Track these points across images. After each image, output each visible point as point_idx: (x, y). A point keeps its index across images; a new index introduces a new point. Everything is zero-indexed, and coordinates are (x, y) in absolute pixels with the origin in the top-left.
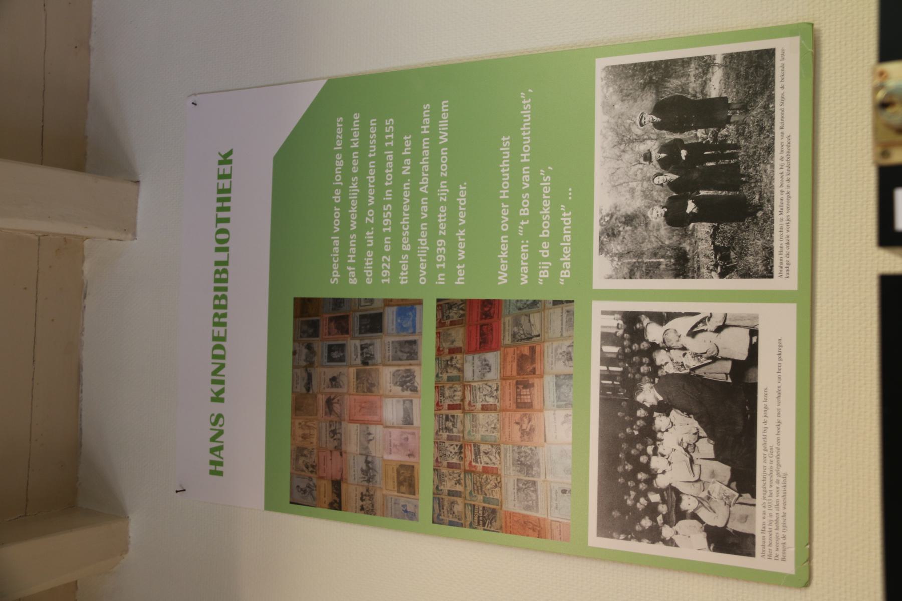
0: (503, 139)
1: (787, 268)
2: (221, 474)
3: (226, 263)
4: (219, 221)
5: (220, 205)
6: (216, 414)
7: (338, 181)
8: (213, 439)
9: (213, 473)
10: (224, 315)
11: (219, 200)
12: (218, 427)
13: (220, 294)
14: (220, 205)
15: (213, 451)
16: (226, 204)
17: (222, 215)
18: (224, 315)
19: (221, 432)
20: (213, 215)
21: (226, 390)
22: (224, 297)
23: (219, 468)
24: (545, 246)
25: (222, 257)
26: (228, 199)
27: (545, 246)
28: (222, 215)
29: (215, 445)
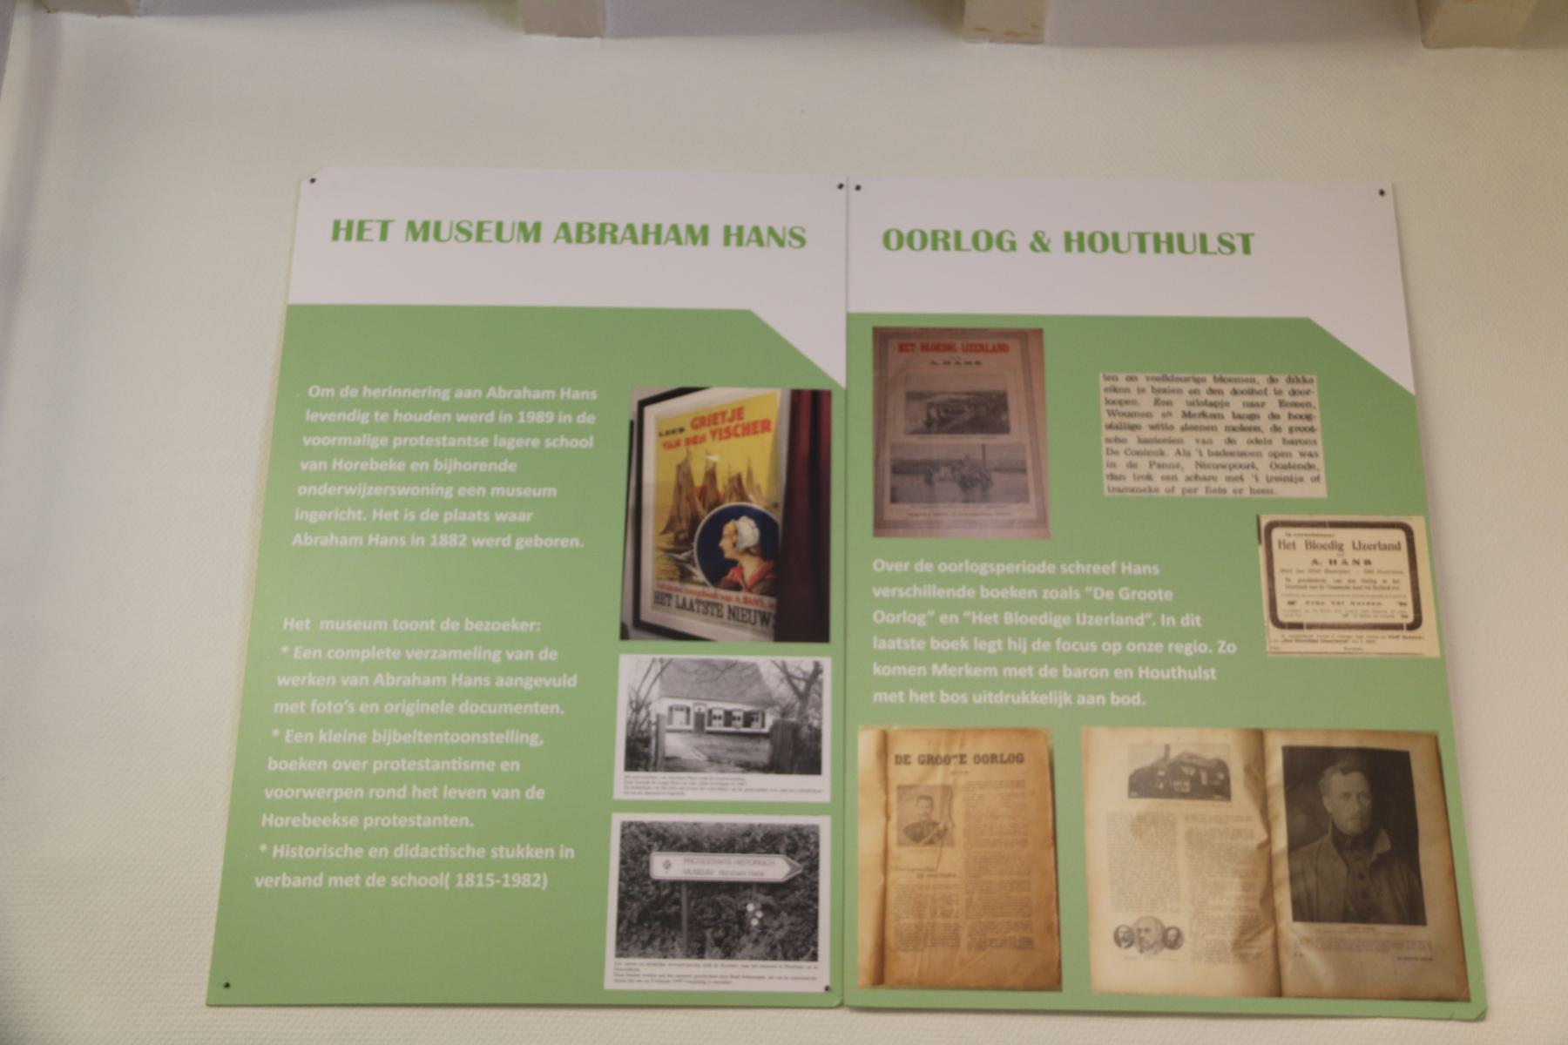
0: (1213, 671)
1: (1290, 479)
2: (336, 237)
3: (958, 247)
4: (1142, 237)
5: (1163, 238)
6: (804, 235)
7: (442, 880)
8: (771, 231)
9: (337, 224)
10: (947, 247)
11: (1169, 236)
12: (788, 238)
13: (596, 232)
14: (1163, 238)
15: (756, 230)
16: (1164, 247)
17: (1149, 241)
18: (947, 247)
19: (781, 243)
20: (1149, 227)
21: (569, 246)
22: (592, 240)
23: (734, 240)
24: (1053, 673)
25: (966, 242)
26: (1170, 250)
27: (1053, 673)
28: (1149, 241)
29: (764, 233)
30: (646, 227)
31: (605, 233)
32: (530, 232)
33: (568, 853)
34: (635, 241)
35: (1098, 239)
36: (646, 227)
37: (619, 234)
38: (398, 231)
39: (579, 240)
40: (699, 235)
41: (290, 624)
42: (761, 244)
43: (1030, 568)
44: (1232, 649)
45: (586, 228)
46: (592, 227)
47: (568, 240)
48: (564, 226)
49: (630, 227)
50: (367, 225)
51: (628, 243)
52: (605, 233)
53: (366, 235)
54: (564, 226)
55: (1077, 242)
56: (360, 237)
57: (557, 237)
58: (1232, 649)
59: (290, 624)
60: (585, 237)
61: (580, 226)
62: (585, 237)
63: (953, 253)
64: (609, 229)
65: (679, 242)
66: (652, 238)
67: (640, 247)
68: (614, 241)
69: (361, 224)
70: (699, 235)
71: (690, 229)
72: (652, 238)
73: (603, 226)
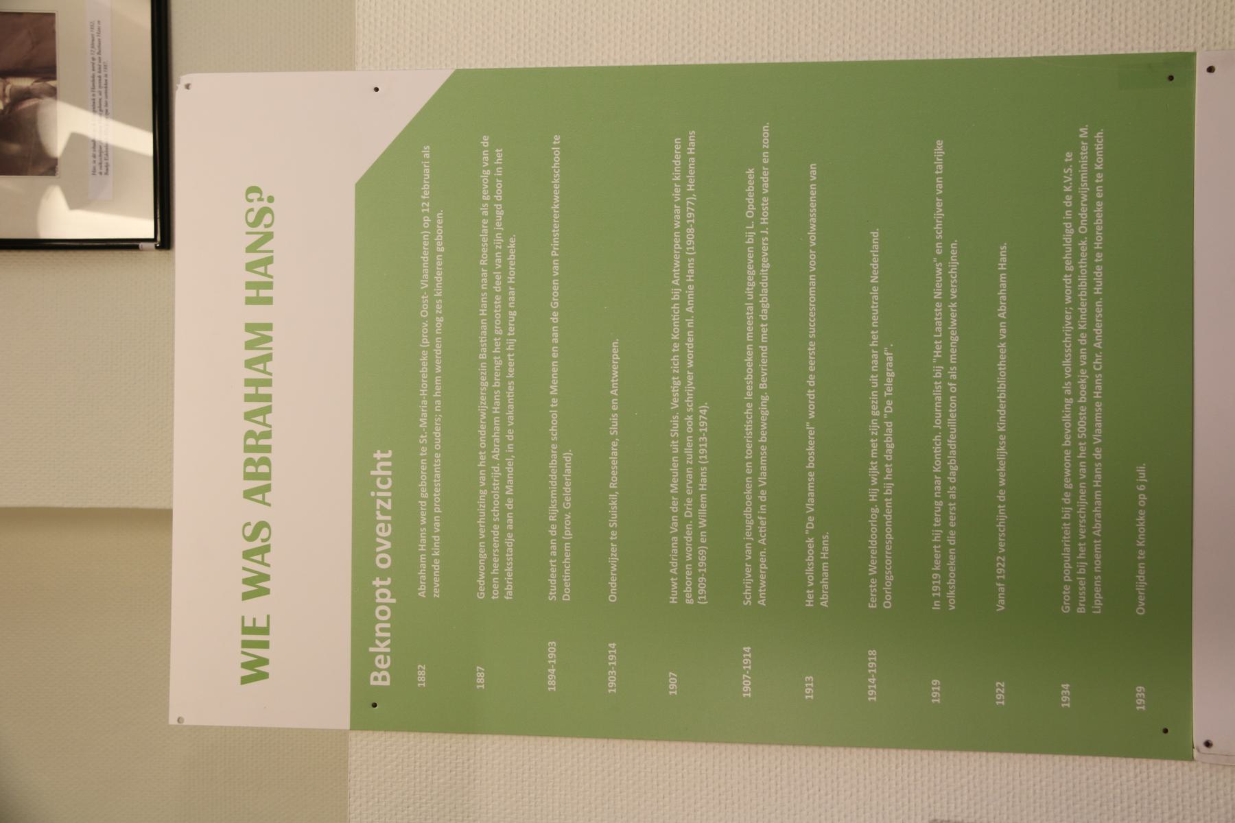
8: (251, 249)
12: (261, 228)
13: (256, 456)
19: (268, 236)
22: (266, 461)
30: (248, 398)
31: (258, 447)
32: (256, 586)
33: (485, 141)
34: (268, 410)
36: (248, 398)
37: (259, 429)
38: (256, 512)
39: (267, 476)
40: (259, 293)
41: (809, 603)
42: (269, 261)
43: (889, 570)
44: (486, 138)
45: (251, 469)
46: (249, 462)
47: (267, 488)
48: (248, 494)
49: (249, 416)
50: (249, 623)
51: (270, 418)
52: (258, 447)
53: (261, 623)
54: (248, 494)
56: (265, 631)
57: (263, 502)
58: (486, 138)
59: (809, 603)
60: (263, 469)
61: (248, 476)
62: (263, 469)
63: (273, 482)
64: (251, 442)
65: (269, 357)
66: (263, 390)
67: (274, 403)
68: (267, 435)
69: (245, 631)
70: (259, 293)
71: (249, 345)
72: (263, 390)
73: (248, 449)
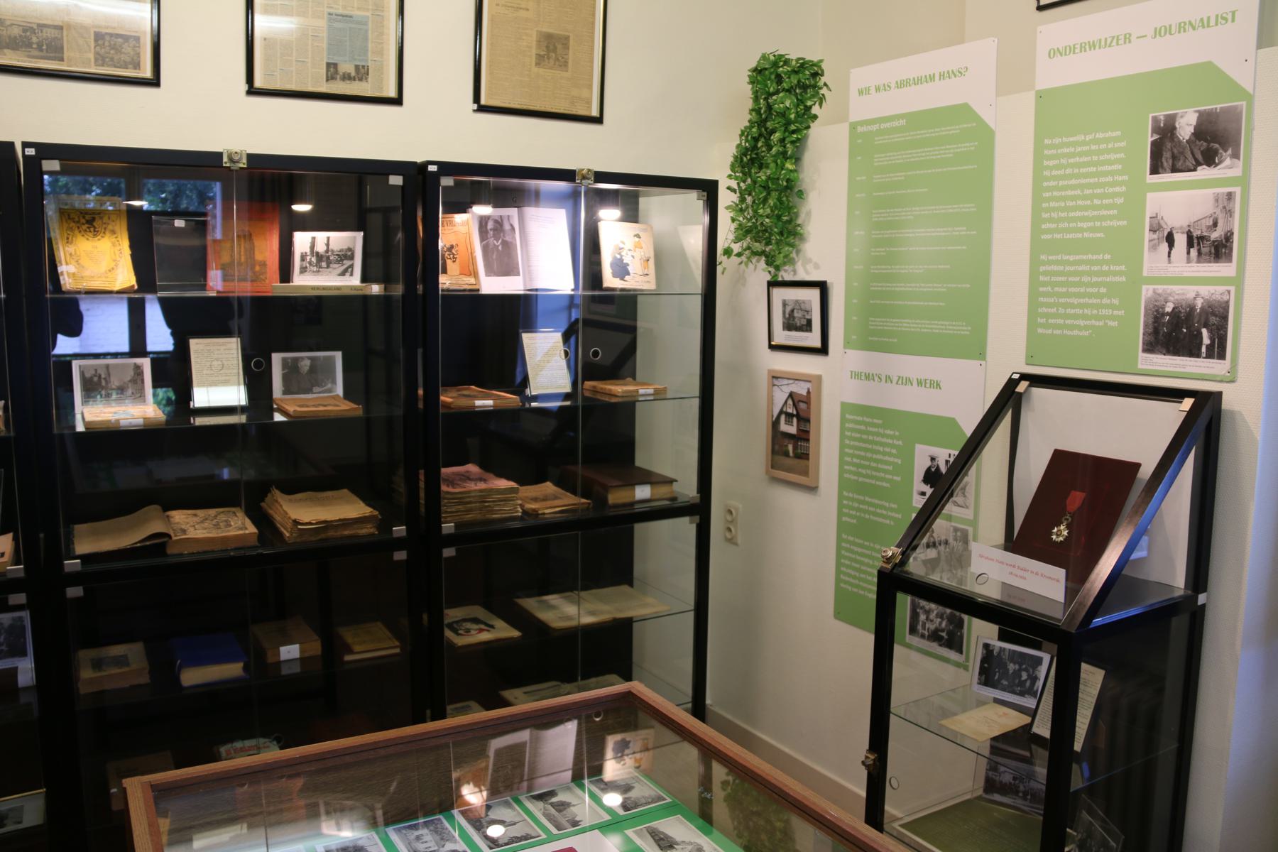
35: (1121, 42)
55: (908, 381)
